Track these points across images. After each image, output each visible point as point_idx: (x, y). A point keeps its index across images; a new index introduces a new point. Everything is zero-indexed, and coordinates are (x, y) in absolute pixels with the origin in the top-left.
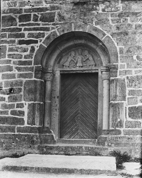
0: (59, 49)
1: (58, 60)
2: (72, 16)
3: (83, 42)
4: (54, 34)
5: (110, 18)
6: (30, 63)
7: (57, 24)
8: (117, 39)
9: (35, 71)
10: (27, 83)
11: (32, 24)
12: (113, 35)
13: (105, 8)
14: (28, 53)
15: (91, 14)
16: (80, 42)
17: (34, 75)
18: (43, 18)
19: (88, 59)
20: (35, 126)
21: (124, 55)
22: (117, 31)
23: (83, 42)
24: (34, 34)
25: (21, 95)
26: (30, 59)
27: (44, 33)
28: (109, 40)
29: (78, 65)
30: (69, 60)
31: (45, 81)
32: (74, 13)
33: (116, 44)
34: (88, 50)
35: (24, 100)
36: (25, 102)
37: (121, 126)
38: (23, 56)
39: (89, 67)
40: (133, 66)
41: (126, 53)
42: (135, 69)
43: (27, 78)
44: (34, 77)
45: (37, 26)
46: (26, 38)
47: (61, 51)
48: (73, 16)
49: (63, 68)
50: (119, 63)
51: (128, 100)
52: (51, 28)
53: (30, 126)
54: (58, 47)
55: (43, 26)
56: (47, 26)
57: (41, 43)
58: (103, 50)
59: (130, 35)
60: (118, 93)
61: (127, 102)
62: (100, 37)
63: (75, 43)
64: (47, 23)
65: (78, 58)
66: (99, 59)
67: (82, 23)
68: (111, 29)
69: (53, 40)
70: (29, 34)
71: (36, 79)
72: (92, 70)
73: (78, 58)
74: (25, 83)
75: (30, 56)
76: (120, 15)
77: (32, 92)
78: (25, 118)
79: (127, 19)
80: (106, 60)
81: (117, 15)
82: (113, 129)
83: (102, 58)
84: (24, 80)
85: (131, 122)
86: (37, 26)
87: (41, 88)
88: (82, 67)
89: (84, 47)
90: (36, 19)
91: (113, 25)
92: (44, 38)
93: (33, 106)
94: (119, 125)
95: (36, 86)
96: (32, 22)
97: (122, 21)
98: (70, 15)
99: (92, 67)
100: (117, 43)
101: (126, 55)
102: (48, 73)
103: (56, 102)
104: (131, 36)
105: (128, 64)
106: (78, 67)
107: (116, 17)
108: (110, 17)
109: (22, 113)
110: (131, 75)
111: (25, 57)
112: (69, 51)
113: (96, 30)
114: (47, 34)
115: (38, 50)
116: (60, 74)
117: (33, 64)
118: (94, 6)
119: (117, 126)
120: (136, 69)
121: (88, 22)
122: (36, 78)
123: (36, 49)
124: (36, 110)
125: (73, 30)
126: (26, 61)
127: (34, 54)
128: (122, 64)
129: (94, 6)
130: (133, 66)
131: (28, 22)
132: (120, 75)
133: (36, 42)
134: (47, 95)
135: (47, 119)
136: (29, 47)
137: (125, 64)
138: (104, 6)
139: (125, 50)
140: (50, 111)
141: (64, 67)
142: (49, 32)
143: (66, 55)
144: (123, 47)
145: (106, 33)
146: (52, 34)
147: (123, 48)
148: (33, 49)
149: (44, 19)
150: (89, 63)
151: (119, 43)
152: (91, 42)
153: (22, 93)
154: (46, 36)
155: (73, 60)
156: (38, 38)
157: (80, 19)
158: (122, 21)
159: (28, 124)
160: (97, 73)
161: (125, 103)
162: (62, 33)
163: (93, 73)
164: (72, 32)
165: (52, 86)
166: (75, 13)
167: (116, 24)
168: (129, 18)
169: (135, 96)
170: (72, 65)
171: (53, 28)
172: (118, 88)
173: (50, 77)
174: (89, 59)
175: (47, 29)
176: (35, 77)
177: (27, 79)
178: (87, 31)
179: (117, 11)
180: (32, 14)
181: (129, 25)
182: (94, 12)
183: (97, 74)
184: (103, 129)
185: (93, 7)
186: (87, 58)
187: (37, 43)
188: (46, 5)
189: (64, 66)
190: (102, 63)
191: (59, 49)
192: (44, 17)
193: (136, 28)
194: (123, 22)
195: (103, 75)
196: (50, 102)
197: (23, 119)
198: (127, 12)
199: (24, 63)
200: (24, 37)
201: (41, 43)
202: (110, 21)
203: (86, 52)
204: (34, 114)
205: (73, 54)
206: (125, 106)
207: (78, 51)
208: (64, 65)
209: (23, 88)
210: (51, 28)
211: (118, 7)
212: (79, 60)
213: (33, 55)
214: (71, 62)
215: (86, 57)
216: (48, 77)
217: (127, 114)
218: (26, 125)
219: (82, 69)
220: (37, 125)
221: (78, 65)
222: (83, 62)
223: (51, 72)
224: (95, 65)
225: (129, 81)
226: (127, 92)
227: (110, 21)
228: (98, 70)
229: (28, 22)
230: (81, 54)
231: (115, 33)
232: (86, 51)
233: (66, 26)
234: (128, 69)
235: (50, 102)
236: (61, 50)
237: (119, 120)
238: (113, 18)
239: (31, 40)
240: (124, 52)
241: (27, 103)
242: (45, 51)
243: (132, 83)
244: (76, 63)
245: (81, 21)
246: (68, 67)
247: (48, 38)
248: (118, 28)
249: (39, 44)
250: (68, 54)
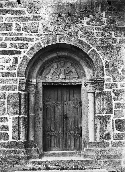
1: (40, 73)
3: (67, 54)
4: (39, 45)
5: (95, 31)
6: (13, 75)
7: (41, 35)
8: (102, 53)
9: (19, 83)
10: (10, 95)
12: (98, 48)
13: (90, 21)
14: (11, 64)
15: (76, 27)
16: (63, 54)
17: (18, 87)
19: (71, 71)
20: (20, 141)
22: (102, 45)
23: (65, 54)
24: (16, 44)
25: (4, 109)
26: (14, 71)
27: (27, 44)
30: (52, 72)
31: (29, 94)
32: (59, 25)
33: (101, 57)
34: (70, 62)
35: (8, 114)
36: (9, 116)
37: (109, 138)
38: (6, 67)
39: (73, 80)
40: (118, 79)
44: (17, 89)
46: (8, 49)
47: (44, 63)
48: (58, 28)
50: (105, 77)
51: (115, 112)
53: (16, 141)
57: (25, 54)
60: (105, 106)
61: (113, 115)
63: (59, 55)
65: (61, 70)
66: (82, 71)
67: (67, 35)
69: (37, 51)
71: (20, 92)
72: (75, 82)
73: (61, 70)
75: (12, 67)
77: (17, 105)
78: (10, 133)
82: (101, 141)
84: (7, 93)
85: (118, 134)
87: (26, 101)
88: (65, 79)
89: (66, 59)
91: (98, 38)
92: (28, 50)
93: (18, 119)
94: (107, 137)
95: (20, 99)
96: (13, 31)
97: (106, 35)
98: (54, 26)
99: (75, 79)
102: (32, 85)
103: (39, 115)
104: (116, 50)
105: (113, 78)
106: (61, 79)
109: (7, 128)
110: (117, 89)
111: (8, 69)
113: (81, 42)
114: (31, 44)
115: (21, 61)
116: (43, 85)
117: (16, 75)
118: (79, 19)
119: (105, 138)
121: (73, 34)
123: (20, 60)
124: (21, 124)
125: (58, 42)
127: (18, 65)
128: (109, 77)
129: (79, 19)
130: (118, 79)
131: (9, 32)
132: (106, 88)
133: (19, 53)
134: (31, 109)
135: (31, 132)
136: (12, 57)
137: (111, 77)
138: (89, 19)
139: (110, 64)
140: (35, 124)
144: (109, 61)
147: (109, 61)
148: (16, 60)
149: (27, 29)
150: (72, 75)
152: (75, 54)
153: (5, 106)
154: (29, 48)
155: (56, 72)
156: (21, 49)
157: (65, 31)
158: (106, 35)
159: (13, 139)
160: (81, 85)
161: (112, 115)
162: (46, 45)
163: (76, 85)
164: (57, 44)
165: (35, 99)
166: (60, 24)
168: (113, 33)
169: (121, 109)
172: (105, 101)
173: (34, 89)
174: (72, 71)
175: (31, 40)
176: (19, 90)
178: (72, 44)
179: (101, 25)
180: (14, 23)
181: (114, 39)
182: (79, 24)
183: (80, 86)
184: (89, 141)
185: (78, 19)
186: (70, 70)
187: (21, 54)
188: (28, 14)
189: (46, 77)
190: (85, 76)
193: (120, 43)
194: (108, 36)
196: (34, 115)
197: (7, 133)
199: (7, 74)
200: (5, 47)
201: (26, 54)
202: (95, 34)
203: (69, 65)
204: (19, 126)
205: (55, 66)
206: (112, 118)
207: (60, 63)
208: (46, 76)
209: (6, 101)
211: (103, 21)
216: (32, 89)
217: (115, 126)
218: (11, 139)
219: (65, 81)
220: (22, 138)
223: (36, 84)
224: (78, 78)
226: (114, 105)
227: (95, 34)
228: (81, 82)
229: (9, 32)
230: (64, 67)
233: (51, 38)
234: (114, 83)
235: (34, 115)
236: (44, 61)
237: (106, 132)
240: (110, 66)
241: (11, 117)
242: (29, 63)
243: (118, 96)
246: (51, 79)
247: (32, 49)
248: (103, 42)
249: (22, 55)
250: (50, 66)
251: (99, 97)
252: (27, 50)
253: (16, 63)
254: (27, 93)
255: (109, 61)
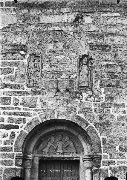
0: (39, 135)
2: (55, 102)
3: (65, 129)
6: (10, 149)
9: (16, 158)
11: (12, 109)
12: (96, 124)
14: (8, 138)
17: (14, 162)
18: (24, 102)
19: (69, 145)
21: (107, 146)
22: (100, 121)
23: (64, 128)
24: (14, 119)
26: (10, 146)
27: (25, 118)
28: (92, 130)
29: (58, 152)
30: (49, 146)
31: (25, 169)
33: (99, 134)
40: (115, 157)
41: (108, 143)
42: (117, 160)
43: (7, 165)
44: (14, 164)
45: (18, 111)
49: (42, 154)
52: (32, 114)
54: (38, 132)
55: (24, 111)
56: (29, 111)
57: (22, 129)
58: (85, 138)
59: (113, 127)
62: (83, 127)
64: (29, 108)
65: (58, 144)
66: (80, 146)
68: (94, 118)
69: (34, 127)
70: (9, 118)
74: (5, 170)
76: (103, 105)
79: (110, 110)
80: (88, 149)
81: (100, 105)
83: (84, 144)
86: (18, 111)
90: (16, 103)
91: (97, 114)
92: (26, 124)
96: (11, 105)
97: (104, 112)
98: (53, 101)
100: (100, 134)
101: (109, 146)
102: (28, 160)
105: (111, 155)
106: (58, 153)
107: (99, 107)
108: (93, 106)
112: (49, 136)
113: (79, 118)
114: (28, 119)
115: (19, 136)
118: (78, 95)
120: (119, 160)
122: (17, 166)
123: (17, 135)
125: (56, 118)
126: (6, 147)
127: (15, 140)
130: (115, 157)
132: (103, 165)
133: (17, 127)
136: (9, 132)
137: (108, 154)
138: (87, 95)
141: (43, 154)
142: (31, 118)
143: (45, 140)
145: (89, 123)
146: (34, 120)
148: (13, 135)
149: (25, 103)
151: (102, 133)
154: (27, 122)
155: (53, 146)
156: (18, 124)
158: (104, 112)
160: (79, 160)
162: (44, 120)
166: (58, 100)
167: (99, 114)
168: (111, 109)
170: (51, 151)
171: (35, 114)
173: (31, 164)
174: (70, 145)
175: (29, 115)
176: (16, 165)
177: (7, 167)
180: (12, 97)
181: (112, 116)
182: (77, 100)
183: (78, 162)
186: (68, 145)
188: (27, 88)
190: (83, 151)
191: (39, 135)
192: (25, 102)
194: (106, 112)
195: (84, 164)
198: (110, 103)
201: (23, 129)
205: (53, 139)
208: (43, 150)
210: (32, 114)
211: (101, 97)
212: (59, 146)
213: (13, 141)
214: (51, 148)
215: (66, 143)
216: (29, 164)
221: (58, 152)
222: (63, 148)
225: (112, 172)
228: (79, 157)
229: (8, 106)
231: (98, 123)
232: (67, 137)
233: (49, 113)
236: (41, 135)
238: (96, 108)
239: (11, 125)
240: (107, 143)
243: (115, 173)
244: (56, 150)
245: (64, 109)
246: (48, 153)
247: (30, 124)
248: (101, 118)
249: (20, 130)
251: (96, 174)
252: (25, 125)
253: (13, 138)
254: (23, 168)
255: (106, 137)
